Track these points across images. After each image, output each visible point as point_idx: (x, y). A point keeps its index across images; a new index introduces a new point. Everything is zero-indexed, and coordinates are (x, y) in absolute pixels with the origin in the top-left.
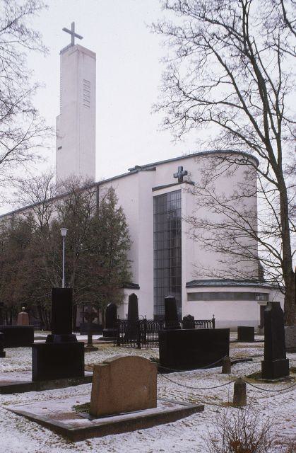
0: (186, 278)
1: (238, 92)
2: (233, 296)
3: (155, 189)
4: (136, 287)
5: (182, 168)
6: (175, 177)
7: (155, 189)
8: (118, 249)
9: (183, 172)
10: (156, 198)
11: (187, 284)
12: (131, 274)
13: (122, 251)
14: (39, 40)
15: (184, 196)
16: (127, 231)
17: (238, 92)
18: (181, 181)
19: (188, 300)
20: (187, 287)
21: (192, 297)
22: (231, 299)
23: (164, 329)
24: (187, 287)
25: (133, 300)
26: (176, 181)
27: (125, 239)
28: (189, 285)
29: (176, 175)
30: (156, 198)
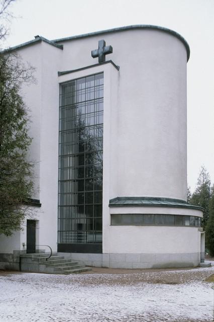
0: (107, 196)
1: (99, 98)
2: (173, 220)
3: (61, 74)
4: (37, 204)
5: (105, 43)
6: (94, 57)
7: (61, 74)
8: (12, 145)
9: (107, 48)
10: (63, 86)
11: (110, 201)
12: (31, 184)
13: (16, 149)
14: (28, 169)
15: (106, 81)
16: (25, 122)
17: (99, 98)
18: (102, 61)
19: (111, 225)
20: (111, 206)
21: (117, 220)
22: (160, 224)
23: (10, 154)
24: (111, 206)
25: (32, 224)
26: (96, 61)
27: (21, 132)
28: (113, 204)
29: (95, 53)
30: (63, 86)
